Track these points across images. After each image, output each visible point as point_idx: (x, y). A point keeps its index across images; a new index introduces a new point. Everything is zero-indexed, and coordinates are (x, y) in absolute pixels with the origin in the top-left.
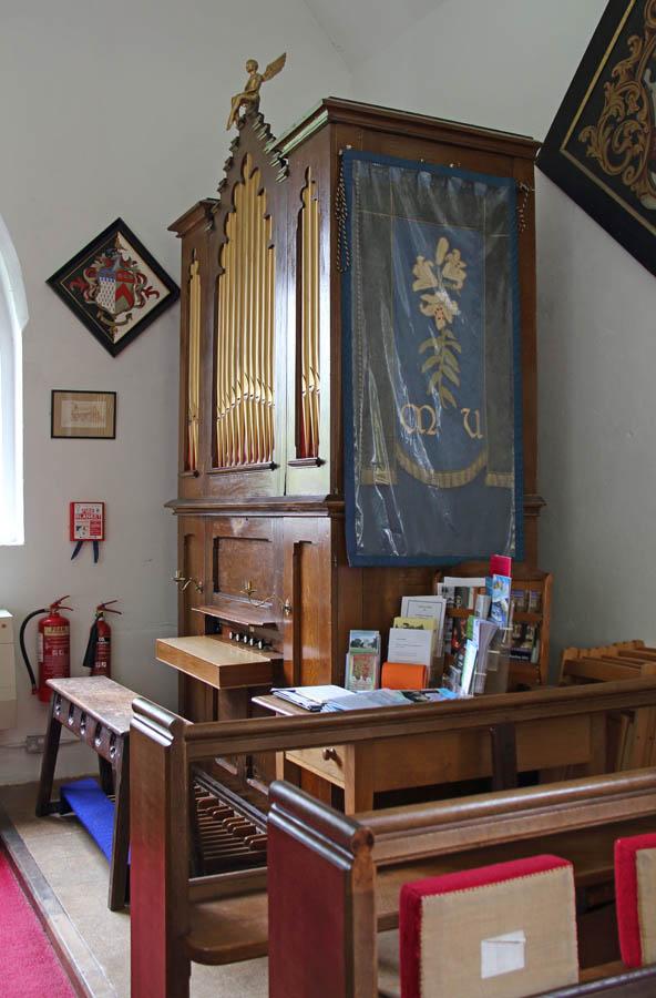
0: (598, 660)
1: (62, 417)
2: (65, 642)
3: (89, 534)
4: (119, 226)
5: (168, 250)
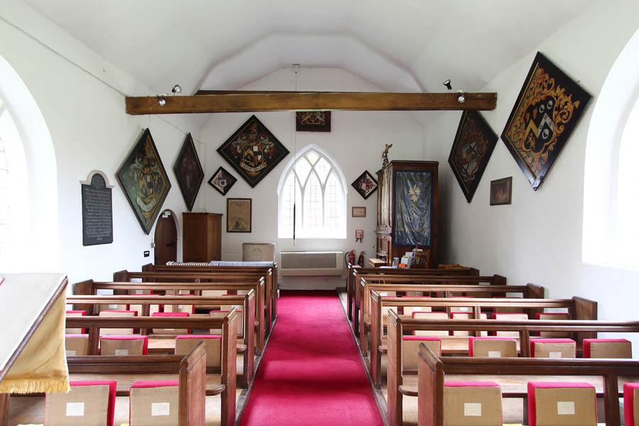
0: (196, 329)
1: (356, 212)
2: (354, 259)
3: (360, 237)
4: (366, 172)
5: (376, 177)
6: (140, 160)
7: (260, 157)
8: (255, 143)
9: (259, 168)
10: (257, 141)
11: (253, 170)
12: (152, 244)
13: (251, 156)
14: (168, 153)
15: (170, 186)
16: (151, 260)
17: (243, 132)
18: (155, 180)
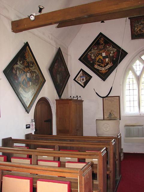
4: (84, 87)
6: (21, 62)
7: (107, 60)
8: (103, 51)
9: (107, 67)
10: (104, 49)
11: (103, 69)
12: (32, 120)
13: (101, 59)
14: (44, 59)
15: (45, 81)
16: (32, 131)
17: (95, 45)
18: (33, 76)
